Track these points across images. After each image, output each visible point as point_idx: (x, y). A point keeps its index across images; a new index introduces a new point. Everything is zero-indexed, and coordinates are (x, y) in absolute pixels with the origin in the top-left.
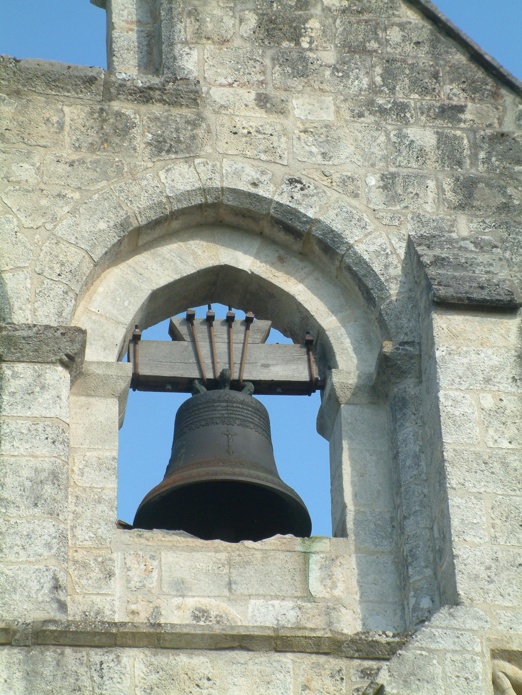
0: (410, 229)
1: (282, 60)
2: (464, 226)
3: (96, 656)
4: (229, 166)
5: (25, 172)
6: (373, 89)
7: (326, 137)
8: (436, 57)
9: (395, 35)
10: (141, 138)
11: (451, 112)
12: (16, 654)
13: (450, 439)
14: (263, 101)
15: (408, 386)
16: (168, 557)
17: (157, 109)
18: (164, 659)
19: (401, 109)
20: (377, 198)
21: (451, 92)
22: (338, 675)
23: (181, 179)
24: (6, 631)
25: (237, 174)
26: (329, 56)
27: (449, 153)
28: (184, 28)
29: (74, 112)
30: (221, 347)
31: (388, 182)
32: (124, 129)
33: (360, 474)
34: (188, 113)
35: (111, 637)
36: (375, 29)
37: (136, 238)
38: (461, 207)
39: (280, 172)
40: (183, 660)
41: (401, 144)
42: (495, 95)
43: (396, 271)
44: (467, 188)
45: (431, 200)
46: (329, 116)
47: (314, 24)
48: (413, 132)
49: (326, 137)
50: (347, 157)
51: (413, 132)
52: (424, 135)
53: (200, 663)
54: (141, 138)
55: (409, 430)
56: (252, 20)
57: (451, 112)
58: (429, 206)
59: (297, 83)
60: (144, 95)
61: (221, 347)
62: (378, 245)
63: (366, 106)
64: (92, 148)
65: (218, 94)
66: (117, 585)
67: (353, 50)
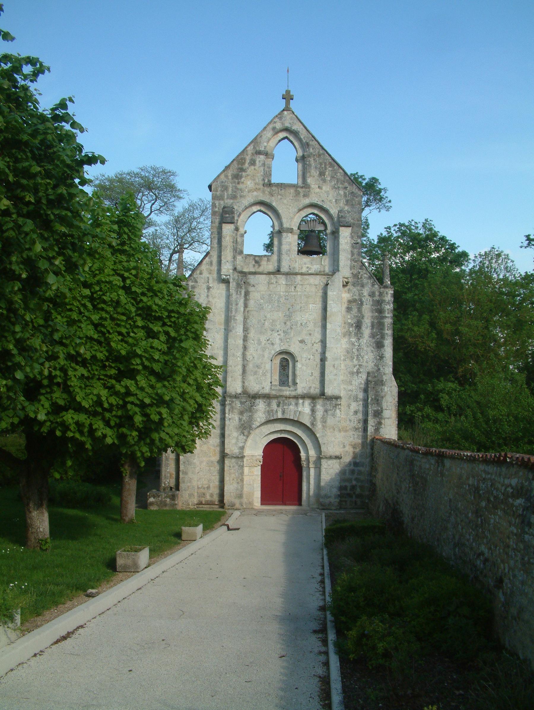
0: (339, 209)
1: (322, 180)
2: (346, 208)
3: (294, 276)
4: (314, 199)
5: (285, 201)
6: (335, 184)
7: (328, 193)
8: (344, 178)
9: (339, 174)
10: (302, 194)
11: (346, 188)
12: (285, 276)
13: (341, 247)
14: (319, 187)
15: (337, 234)
16: (304, 259)
17: (304, 189)
18: (302, 276)
19: (339, 187)
20: (334, 203)
21: (346, 184)
22: (324, 278)
23: (307, 201)
24: (324, 706)
25: (315, 200)
26: (329, 179)
27: (345, 195)
28: (308, 175)
29: (292, 191)
30: (312, 225)
31: (336, 200)
32: (299, 193)
33: (330, 246)
34: (308, 190)
35: (296, 274)
36: (336, 173)
37: (300, 210)
38: (346, 205)
39: (321, 199)
40: (305, 276)
41: (338, 194)
42: (352, 185)
43: (336, 216)
44: (347, 201)
45: (342, 204)
46: (328, 190)
47: (327, 173)
48: (340, 192)
49: (328, 193)
50: (330, 197)
51: (340, 192)
52: (342, 192)
53: (307, 277)
54: (302, 194)
55: (336, 242)
56: (318, 172)
57: (346, 188)
58: (341, 205)
59: (324, 184)
60: (302, 187)
61: (312, 225)
62: (334, 211)
63: (334, 187)
64: (295, 197)
65: (312, 186)
66: (297, 263)
67: (332, 177)
